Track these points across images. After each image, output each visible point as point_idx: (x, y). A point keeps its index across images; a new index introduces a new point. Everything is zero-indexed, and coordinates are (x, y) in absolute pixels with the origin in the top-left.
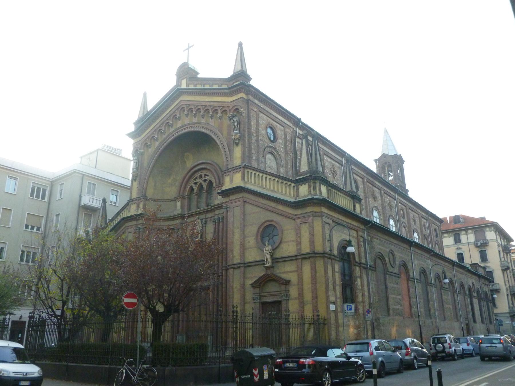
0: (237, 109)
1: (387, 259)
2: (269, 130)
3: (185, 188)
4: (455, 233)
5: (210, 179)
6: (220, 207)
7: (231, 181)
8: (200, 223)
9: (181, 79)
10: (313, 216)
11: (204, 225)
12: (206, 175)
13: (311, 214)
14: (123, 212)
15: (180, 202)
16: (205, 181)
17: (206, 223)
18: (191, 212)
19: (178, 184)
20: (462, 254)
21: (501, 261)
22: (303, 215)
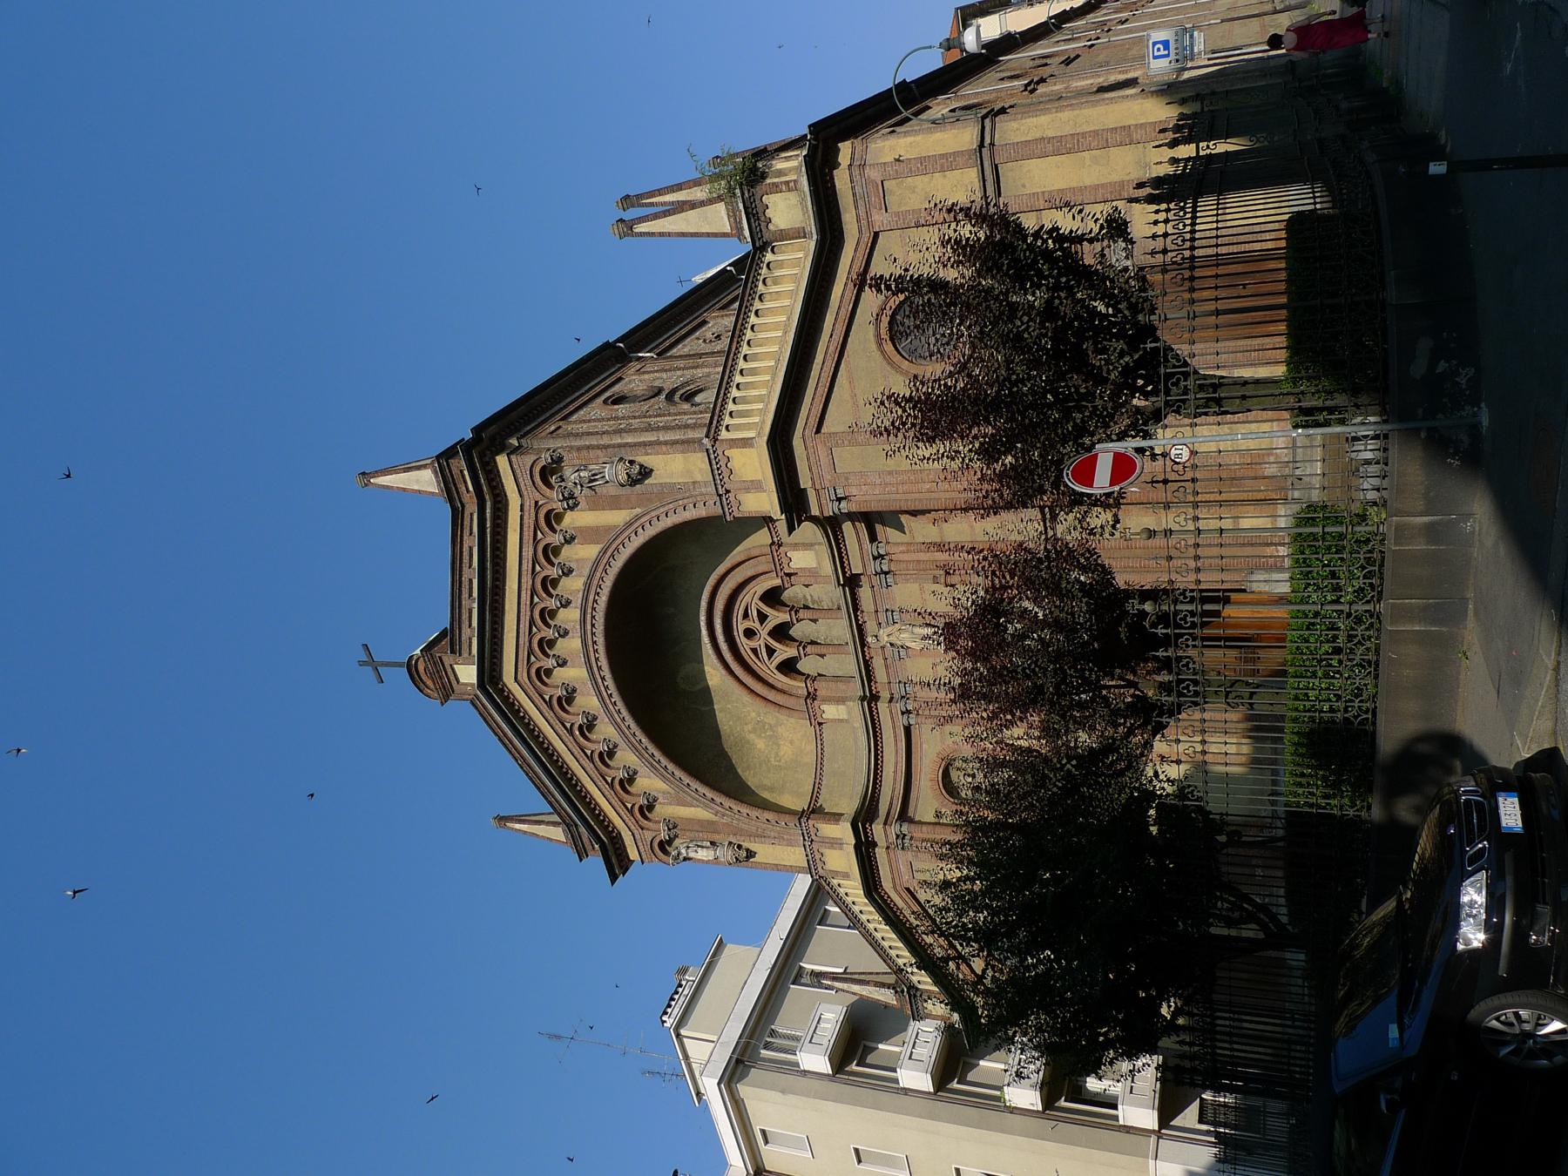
0: (543, 471)
5: (756, 600)
7: (756, 486)
10: (863, 166)
12: (746, 616)
13: (856, 172)
14: (849, 900)
15: (824, 707)
16: (762, 617)
19: (770, 716)
22: (861, 202)
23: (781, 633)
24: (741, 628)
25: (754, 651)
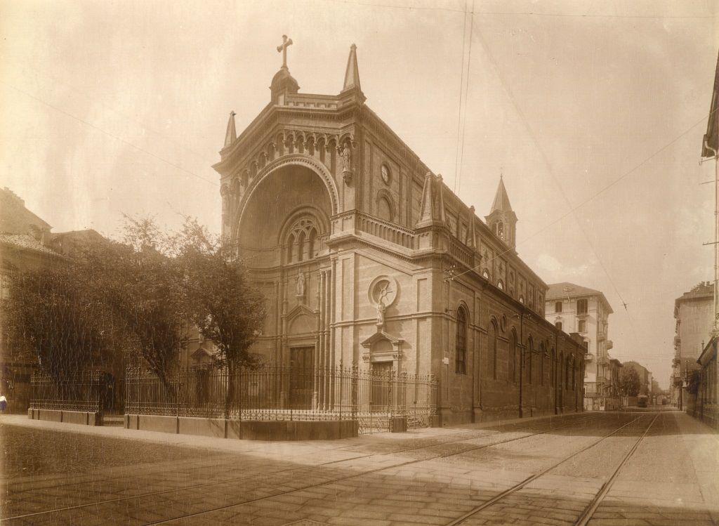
1: (499, 323)
2: (384, 169)
3: (284, 239)
4: (556, 301)
6: (326, 259)
8: (303, 276)
9: (277, 94)
11: (307, 280)
12: (309, 222)
17: (310, 278)
18: (303, 261)
20: (561, 323)
21: (598, 332)
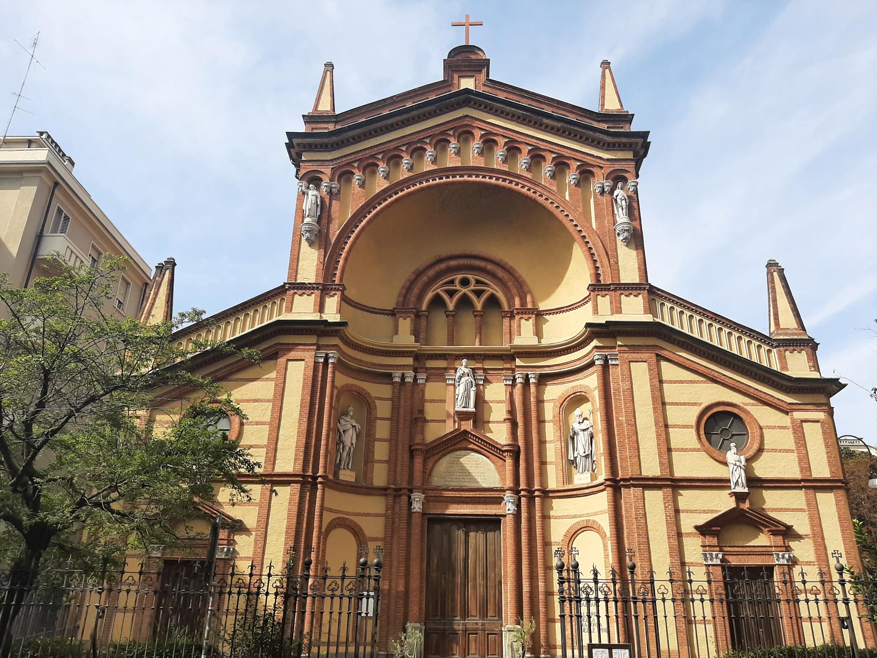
5: (491, 290)
12: (478, 282)
23: (465, 303)
24: (470, 277)
25: (452, 282)
